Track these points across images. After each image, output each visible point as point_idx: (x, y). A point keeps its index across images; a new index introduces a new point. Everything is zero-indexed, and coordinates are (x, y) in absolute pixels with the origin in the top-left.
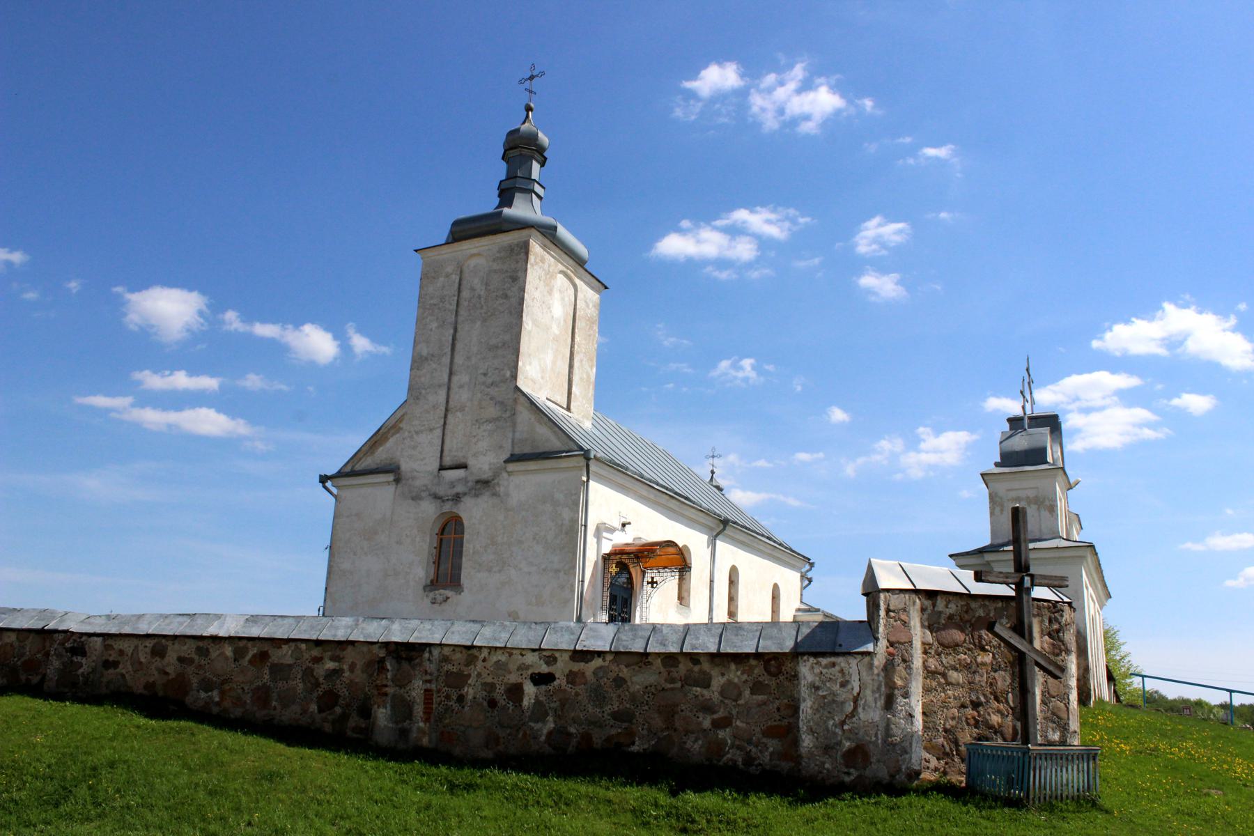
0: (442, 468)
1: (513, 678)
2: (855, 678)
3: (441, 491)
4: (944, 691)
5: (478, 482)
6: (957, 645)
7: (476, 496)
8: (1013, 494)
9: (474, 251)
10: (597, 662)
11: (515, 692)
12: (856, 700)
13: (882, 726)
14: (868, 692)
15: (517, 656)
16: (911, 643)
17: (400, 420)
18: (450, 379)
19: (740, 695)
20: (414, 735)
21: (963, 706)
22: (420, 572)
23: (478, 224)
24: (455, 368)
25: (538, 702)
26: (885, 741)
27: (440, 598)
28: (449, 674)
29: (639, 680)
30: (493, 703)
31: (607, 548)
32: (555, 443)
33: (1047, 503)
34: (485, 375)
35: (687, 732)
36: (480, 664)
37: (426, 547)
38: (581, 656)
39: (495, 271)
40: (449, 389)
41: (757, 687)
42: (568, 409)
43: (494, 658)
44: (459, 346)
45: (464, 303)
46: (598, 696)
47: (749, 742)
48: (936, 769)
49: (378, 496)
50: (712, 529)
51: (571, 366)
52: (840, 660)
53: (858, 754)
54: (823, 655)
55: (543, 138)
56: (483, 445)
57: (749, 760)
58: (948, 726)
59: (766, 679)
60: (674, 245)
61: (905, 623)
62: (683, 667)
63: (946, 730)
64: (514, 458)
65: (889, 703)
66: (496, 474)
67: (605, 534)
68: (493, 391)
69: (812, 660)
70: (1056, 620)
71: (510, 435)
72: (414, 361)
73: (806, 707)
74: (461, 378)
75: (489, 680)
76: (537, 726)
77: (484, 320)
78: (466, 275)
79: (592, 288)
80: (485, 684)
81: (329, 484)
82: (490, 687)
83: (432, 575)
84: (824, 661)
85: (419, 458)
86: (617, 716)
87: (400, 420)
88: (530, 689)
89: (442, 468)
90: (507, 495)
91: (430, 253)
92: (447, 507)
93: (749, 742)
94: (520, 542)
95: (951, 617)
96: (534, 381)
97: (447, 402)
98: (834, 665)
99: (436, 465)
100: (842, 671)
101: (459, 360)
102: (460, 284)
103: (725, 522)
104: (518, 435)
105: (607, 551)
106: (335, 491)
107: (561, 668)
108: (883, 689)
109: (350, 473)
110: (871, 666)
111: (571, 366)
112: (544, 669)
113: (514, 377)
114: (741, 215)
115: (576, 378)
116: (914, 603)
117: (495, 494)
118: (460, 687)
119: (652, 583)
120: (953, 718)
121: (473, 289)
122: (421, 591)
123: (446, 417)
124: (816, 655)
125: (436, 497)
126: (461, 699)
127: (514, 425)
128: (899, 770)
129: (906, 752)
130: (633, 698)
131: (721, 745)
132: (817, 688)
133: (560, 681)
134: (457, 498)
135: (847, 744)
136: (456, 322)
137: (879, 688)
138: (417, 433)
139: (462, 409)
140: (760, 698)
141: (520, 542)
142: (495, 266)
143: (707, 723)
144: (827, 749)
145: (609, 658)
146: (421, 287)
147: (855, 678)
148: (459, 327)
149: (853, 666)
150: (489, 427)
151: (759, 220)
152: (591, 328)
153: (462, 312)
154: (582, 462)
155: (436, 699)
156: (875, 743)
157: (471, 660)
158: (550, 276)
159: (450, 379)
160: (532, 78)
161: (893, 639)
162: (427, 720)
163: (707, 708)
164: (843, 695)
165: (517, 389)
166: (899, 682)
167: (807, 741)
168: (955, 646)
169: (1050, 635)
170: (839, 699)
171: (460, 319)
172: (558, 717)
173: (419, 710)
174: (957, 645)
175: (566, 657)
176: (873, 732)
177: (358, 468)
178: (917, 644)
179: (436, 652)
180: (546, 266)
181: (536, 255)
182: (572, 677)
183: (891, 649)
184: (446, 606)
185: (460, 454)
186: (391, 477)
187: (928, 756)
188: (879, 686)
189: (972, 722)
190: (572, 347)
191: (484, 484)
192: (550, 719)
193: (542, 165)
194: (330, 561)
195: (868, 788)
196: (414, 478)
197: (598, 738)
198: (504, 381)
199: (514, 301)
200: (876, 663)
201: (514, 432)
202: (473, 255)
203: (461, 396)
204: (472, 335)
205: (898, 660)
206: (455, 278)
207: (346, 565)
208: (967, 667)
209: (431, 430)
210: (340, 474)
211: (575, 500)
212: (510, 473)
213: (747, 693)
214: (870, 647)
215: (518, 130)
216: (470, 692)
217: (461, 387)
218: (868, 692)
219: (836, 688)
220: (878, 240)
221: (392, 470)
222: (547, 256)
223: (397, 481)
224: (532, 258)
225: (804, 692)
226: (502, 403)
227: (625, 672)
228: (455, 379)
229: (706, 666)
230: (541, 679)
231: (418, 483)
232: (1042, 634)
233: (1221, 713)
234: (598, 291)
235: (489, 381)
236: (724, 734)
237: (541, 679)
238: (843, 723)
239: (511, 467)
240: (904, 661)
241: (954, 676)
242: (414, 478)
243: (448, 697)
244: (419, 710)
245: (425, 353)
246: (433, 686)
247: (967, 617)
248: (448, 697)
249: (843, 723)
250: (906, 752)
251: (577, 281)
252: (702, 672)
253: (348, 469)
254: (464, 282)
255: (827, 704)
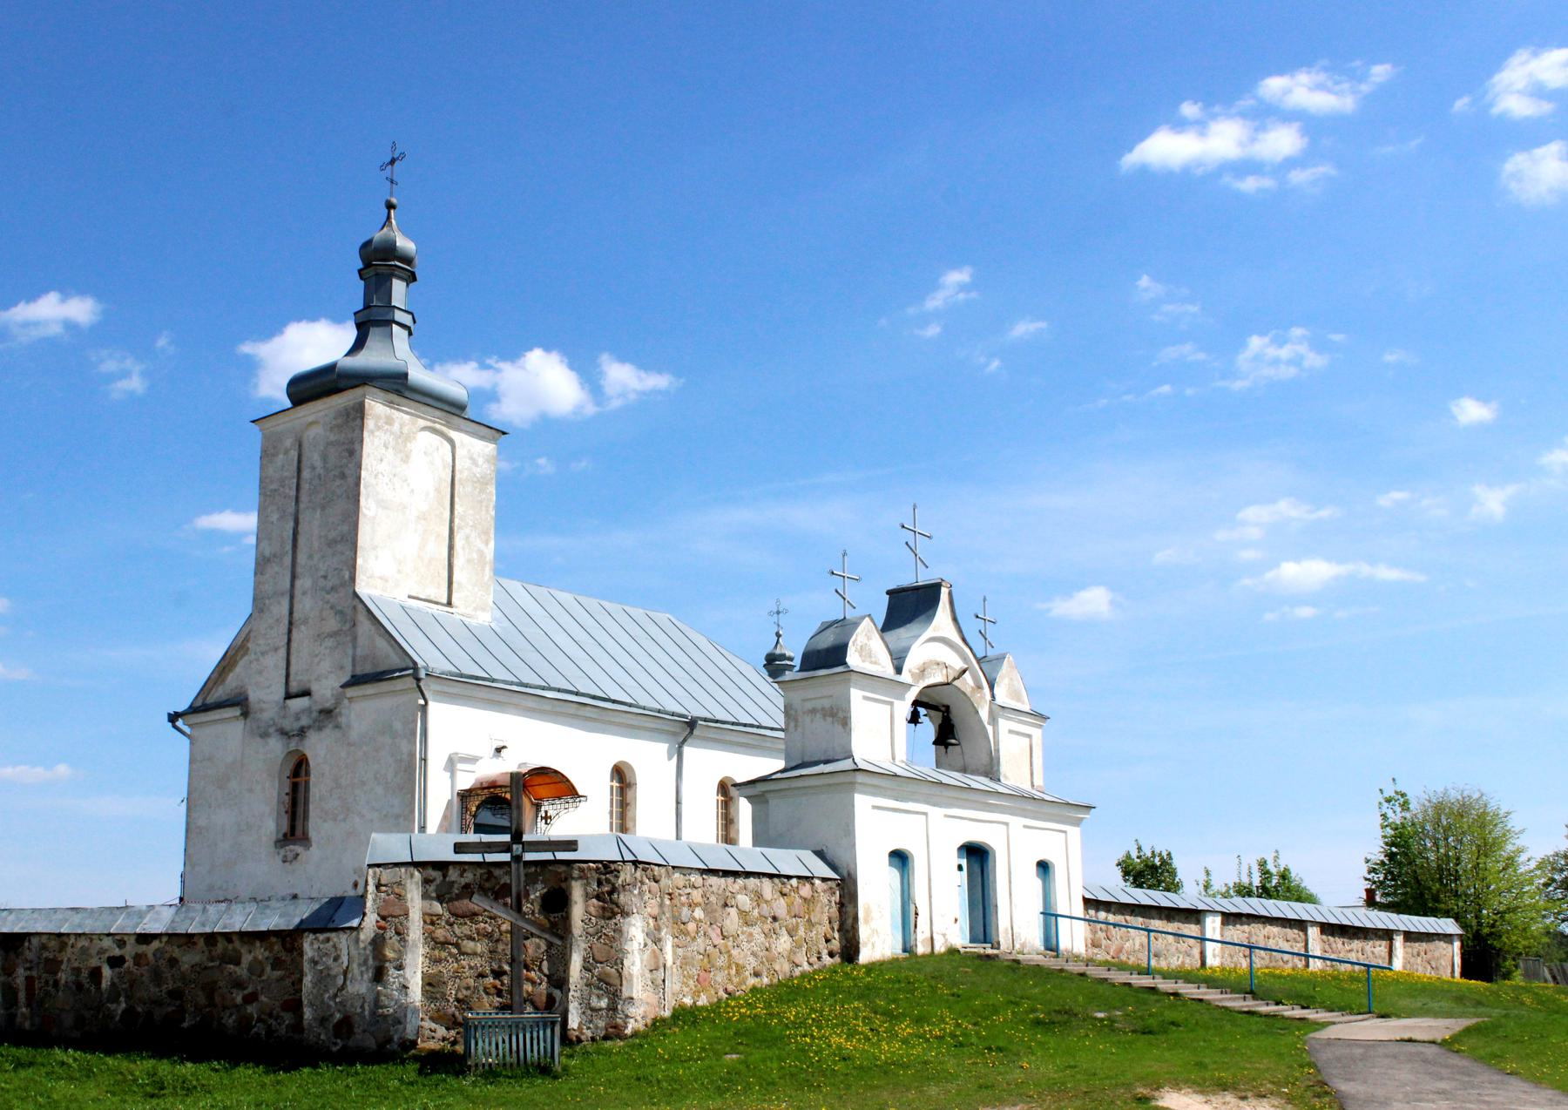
0: (288, 696)
1: (94, 962)
2: (345, 952)
3: (288, 724)
4: (457, 961)
5: (321, 712)
6: (475, 914)
7: (320, 729)
8: (809, 706)
9: (311, 418)
10: (156, 944)
11: (96, 973)
12: (345, 973)
13: (370, 998)
14: (355, 966)
15: (96, 941)
16: (407, 915)
17: (247, 639)
18: (292, 585)
19: (263, 971)
20: (18, 1020)
21: (482, 975)
22: (271, 826)
23: (313, 383)
24: (299, 570)
25: (113, 984)
26: (373, 1013)
27: (290, 856)
28: (47, 959)
29: (188, 959)
30: (79, 986)
31: (466, 782)
32: (395, 660)
33: (841, 715)
34: (325, 577)
35: (225, 1008)
36: (69, 950)
37: (275, 794)
38: (145, 938)
39: (331, 444)
40: (292, 597)
41: (277, 963)
42: (449, 604)
43: (80, 945)
44: (302, 541)
45: (305, 486)
46: (157, 977)
47: (270, 1015)
48: (444, 1039)
49: (228, 732)
50: (674, 734)
51: (451, 548)
52: (333, 935)
53: (345, 1026)
54: (322, 931)
55: (404, 244)
56: (326, 665)
57: (270, 1031)
58: (460, 996)
59: (284, 955)
60: (1165, 148)
61: (399, 897)
62: (221, 945)
63: (458, 1000)
64: (356, 680)
65: (379, 975)
66: (338, 701)
67: (460, 766)
68: (333, 598)
69: (312, 936)
70: (608, 881)
71: (350, 652)
72: (257, 564)
73: (308, 980)
74: (304, 583)
75: (76, 965)
76: (113, 1006)
77: (323, 508)
78: (306, 445)
79: (482, 438)
80: (73, 969)
81: (180, 723)
82: (77, 971)
83: (285, 827)
84: (321, 937)
85: (266, 690)
86: (171, 993)
87: (247, 639)
88: (107, 972)
89: (288, 696)
90: (349, 726)
91: (268, 424)
92: (293, 746)
93: (270, 1015)
94: (363, 783)
95: (467, 886)
96: (384, 579)
97: (291, 613)
98: (328, 940)
99: (283, 695)
100: (334, 946)
101: (302, 558)
102: (299, 462)
103: (692, 724)
104: (359, 652)
105: (467, 786)
106: (186, 729)
107: (130, 950)
108: (371, 961)
109: (200, 708)
110: (357, 940)
111: (451, 548)
112: (117, 952)
113: (353, 579)
114: (1274, 85)
115: (457, 563)
116: (412, 876)
117: (338, 727)
118: (56, 973)
119: (547, 818)
120: (468, 988)
121: (313, 468)
122: (272, 849)
123: (290, 631)
124: (315, 931)
125: (283, 733)
126: (56, 983)
127: (355, 639)
128: (390, 1040)
129: (400, 1023)
130: (183, 978)
131: (249, 1018)
132: (316, 963)
133: (129, 964)
134: (302, 733)
135: (338, 1016)
136: (297, 511)
137: (365, 962)
138: (263, 654)
139: (305, 622)
140: (278, 973)
141: (363, 783)
142: (332, 437)
143: (239, 1000)
144: (323, 1021)
145: (165, 939)
146: (262, 468)
147: (345, 952)
148: (301, 517)
149: (342, 940)
150: (330, 643)
151: (1300, 90)
152: (482, 491)
153: (304, 498)
154: (411, 682)
155: (37, 985)
156: (362, 1014)
157: (63, 946)
158: (404, 438)
159: (292, 585)
160: (393, 162)
161: (384, 913)
162: (28, 1005)
163: (239, 984)
164: (336, 970)
165: (356, 595)
166: (390, 954)
167: (308, 1014)
168: (473, 916)
169: (598, 897)
170: (333, 973)
171: (302, 506)
172: (128, 998)
173: (22, 996)
174: (475, 914)
175: (132, 939)
176: (358, 1004)
177: (210, 700)
178: (415, 916)
179: (35, 941)
180: (396, 427)
181: (378, 418)
182: (138, 958)
183: (382, 923)
184: (296, 865)
185: (305, 678)
186: (237, 711)
187: (433, 1026)
188: (365, 962)
189: (493, 991)
190: (452, 521)
191: (327, 714)
192: (122, 999)
193: (411, 278)
194: (188, 816)
195: (349, 1056)
196: (262, 710)
197: (158, 1013)
198: (343, 585)
199: (351, 480)
200: (362, 937)
201: (355, 647)
202: (311, 424)
203: (305, 605)
204: (312, 525)
205: (390, 933)
206: (294, 454)
207: (202, 822)
208: (489, 936)
209: (276, 649)
210: (193, 710)
211: (413, 727)
212: (350, 699)
213: (268, 969)
214: (355, 923)
215: (369, 242)
216: (63, 977)
217: (304, 593)
218: (355, 966)
219: (330, 962)
220: (1538, 91)
221: (240, 703)
222: (396, 414)
223: (245, 715)
224: (370, 423)
225: (306, 967)
226: (341, 612)
227: (176, 953)
228: (298, 583)
229: (237, 944)
230: (115, 962)
231: (266, 716)
232: (587, 897)
233: (1545, 940)
234: (493, 440)
235: (330, 584)
236: (251, 1009)
237: (115, 962)
238: (336, 995)
239: (350, 692)
240: (398, 933)
241: (469, 945)
242: (262, 710)
243: (47, 982)
244: (22, 996)
245: (267, 554)
246: (34, 973)
247: (487, 885)
248: (47, 982)
249: (336, 995)
250: (400, 1023)
251: (453, 434)
252: (234, 950)
253: (199, 703)
254: (304, 459)
255: (324, 978)
